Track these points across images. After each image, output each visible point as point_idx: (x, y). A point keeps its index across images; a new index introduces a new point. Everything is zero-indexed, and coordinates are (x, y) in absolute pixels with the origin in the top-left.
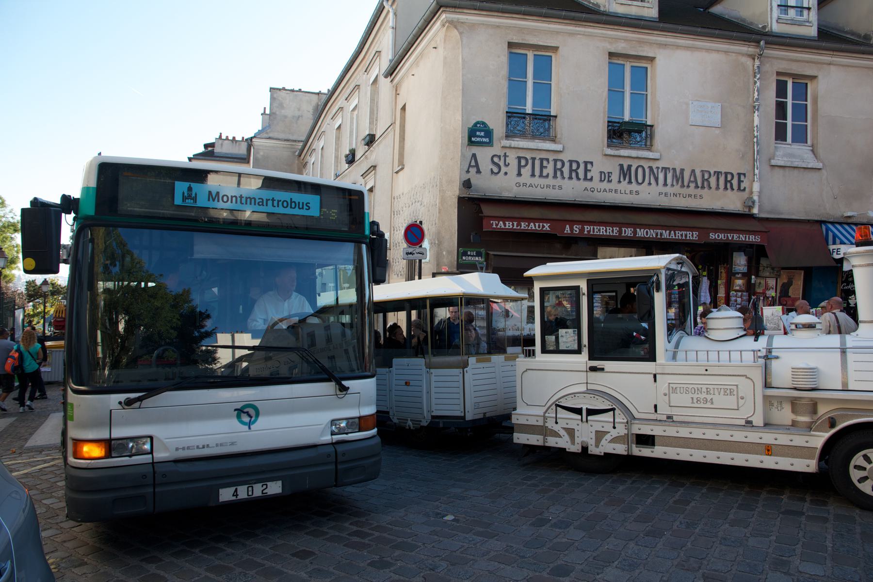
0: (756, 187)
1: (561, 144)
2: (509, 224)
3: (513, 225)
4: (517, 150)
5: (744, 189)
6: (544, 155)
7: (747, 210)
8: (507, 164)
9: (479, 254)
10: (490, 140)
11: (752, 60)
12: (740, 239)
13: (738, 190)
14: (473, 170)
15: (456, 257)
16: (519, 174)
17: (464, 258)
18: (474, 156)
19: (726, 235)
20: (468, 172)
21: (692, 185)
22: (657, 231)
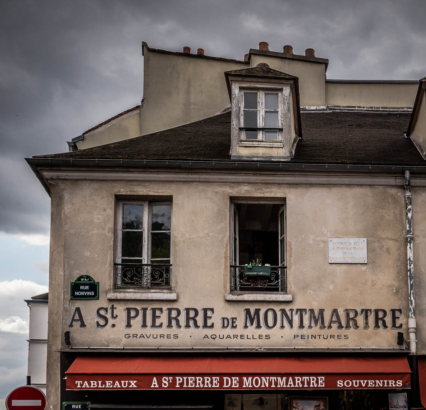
3: (98, 384)
8: (115, 316)
16: (129, 325)
21: (335, 326)
22: (271, 378)
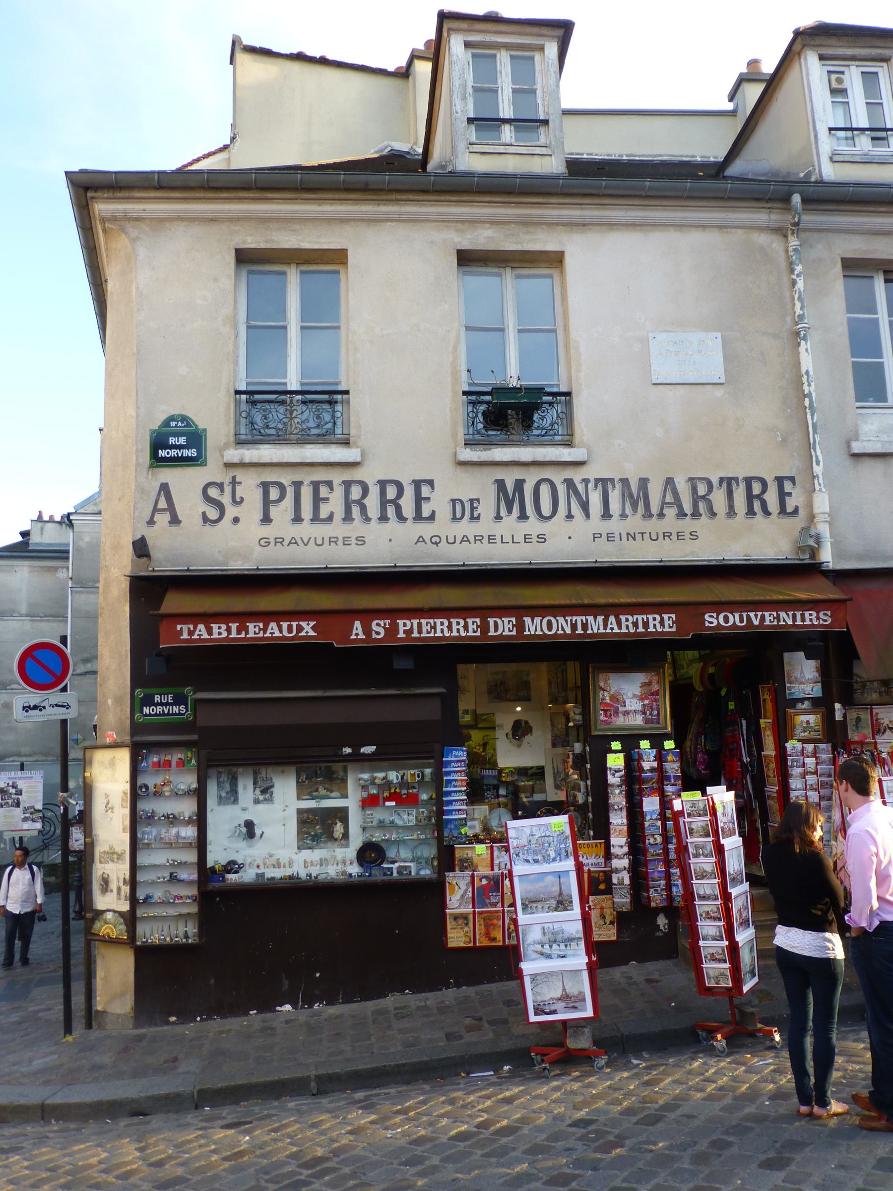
0: (822, 503)
1: (357, 447)
2: (219, 628)
3: (229, 630)
4: (260, 470)
5: (796, 511)
6: (320, 475)
7: (806, 558)
8: (238, 500)
9: (179, 700)
10: (199, 452)
11: (781, 238)
12: (782, 623)
13: (779, 514)
14: (163, 519)
15: (128, 710)
16: (266, 519)
17: (146, 710)
18: (165, 488)
19: (745, 615)
20: (151, 522)
21: (671, 512)
22: (574, 618)
